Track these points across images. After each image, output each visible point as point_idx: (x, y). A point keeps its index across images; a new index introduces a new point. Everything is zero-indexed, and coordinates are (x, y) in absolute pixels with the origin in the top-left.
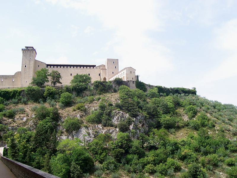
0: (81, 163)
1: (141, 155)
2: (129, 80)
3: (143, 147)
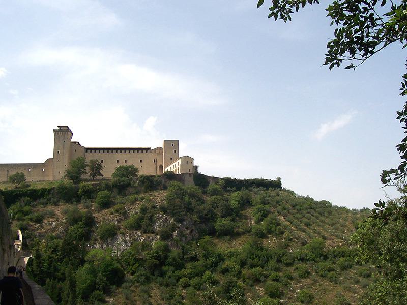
0: (109, 274)
1: (179, 266)
2: (184, 172)
3: (183, 259)
